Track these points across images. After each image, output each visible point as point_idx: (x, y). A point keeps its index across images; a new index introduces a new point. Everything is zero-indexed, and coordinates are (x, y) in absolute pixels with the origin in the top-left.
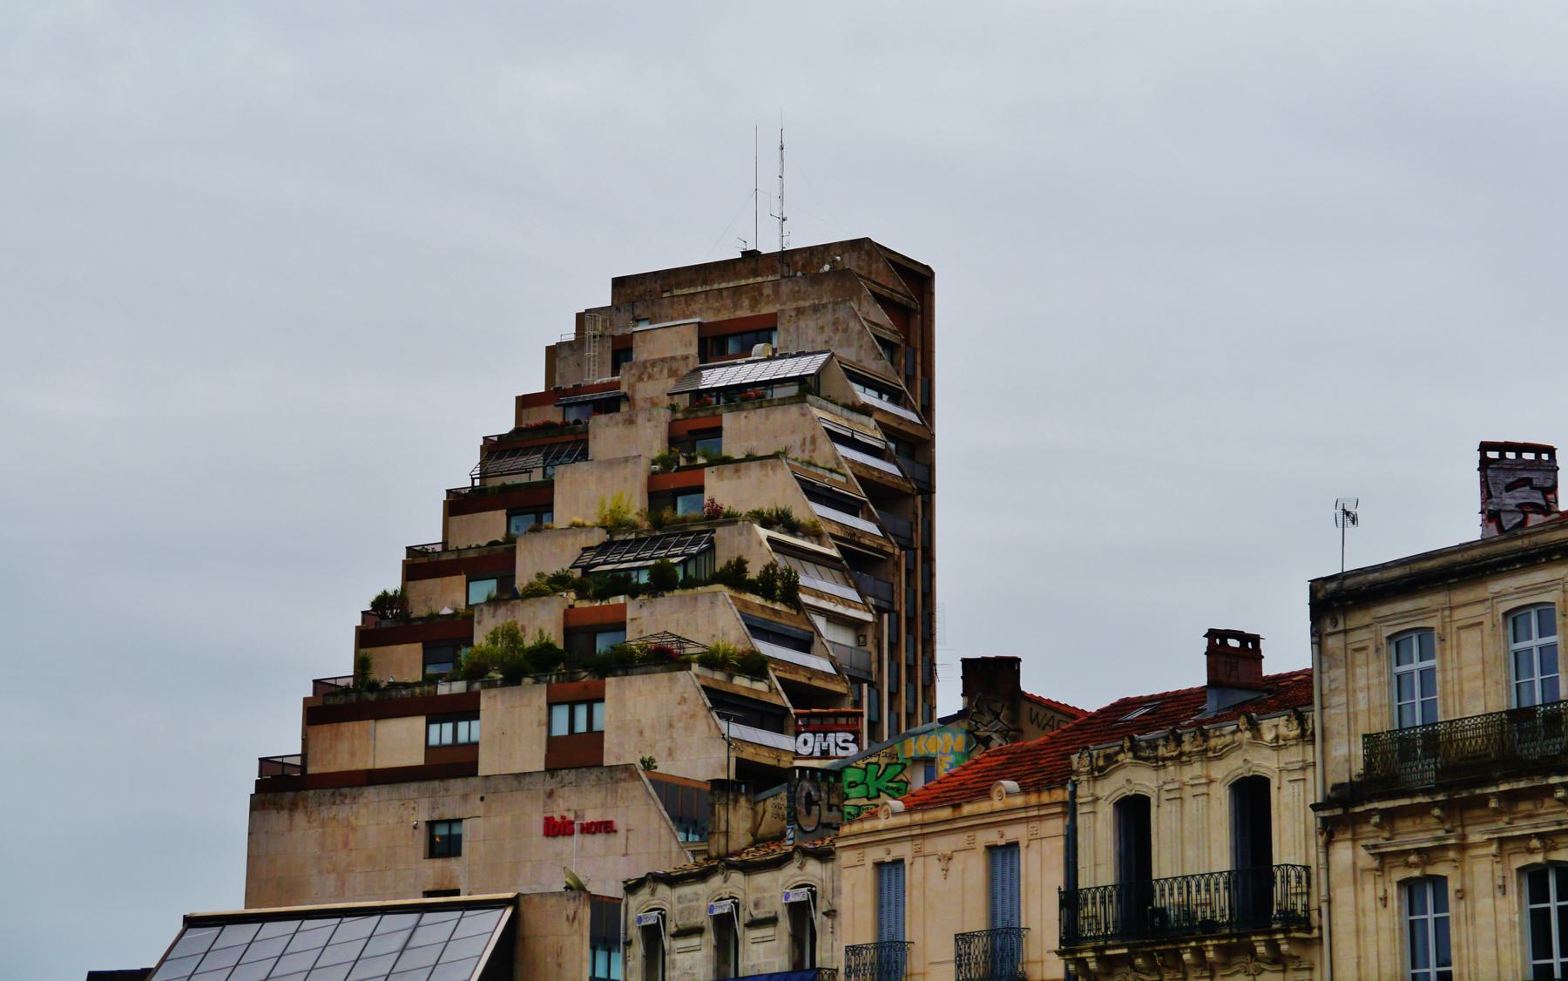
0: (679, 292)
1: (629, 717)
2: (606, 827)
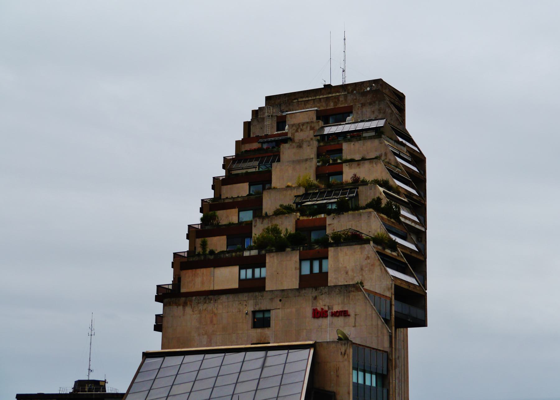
0: (301, 100)
1: (340, 265)
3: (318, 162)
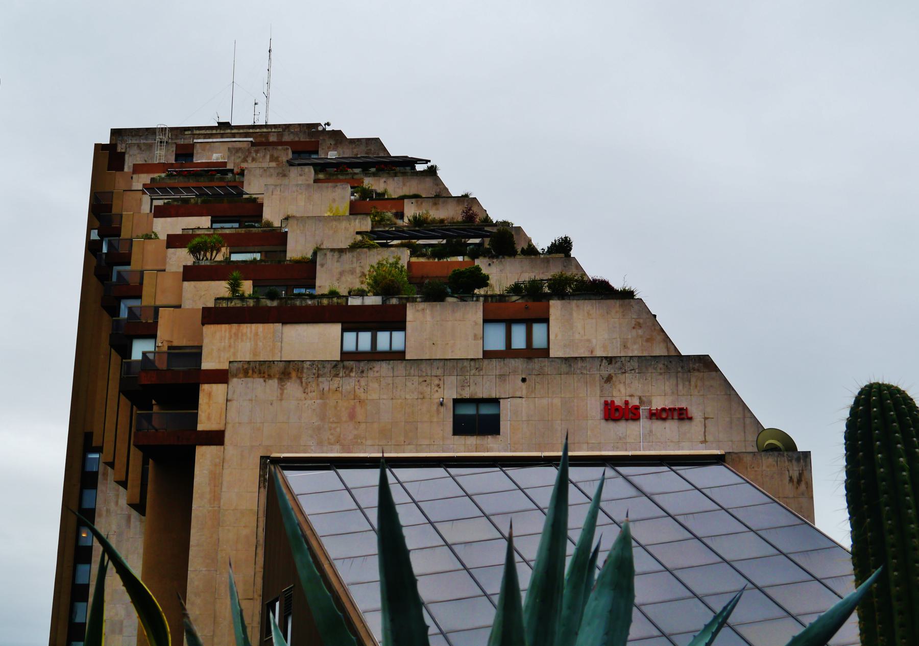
1: (577, 336)
3: (352, 194)
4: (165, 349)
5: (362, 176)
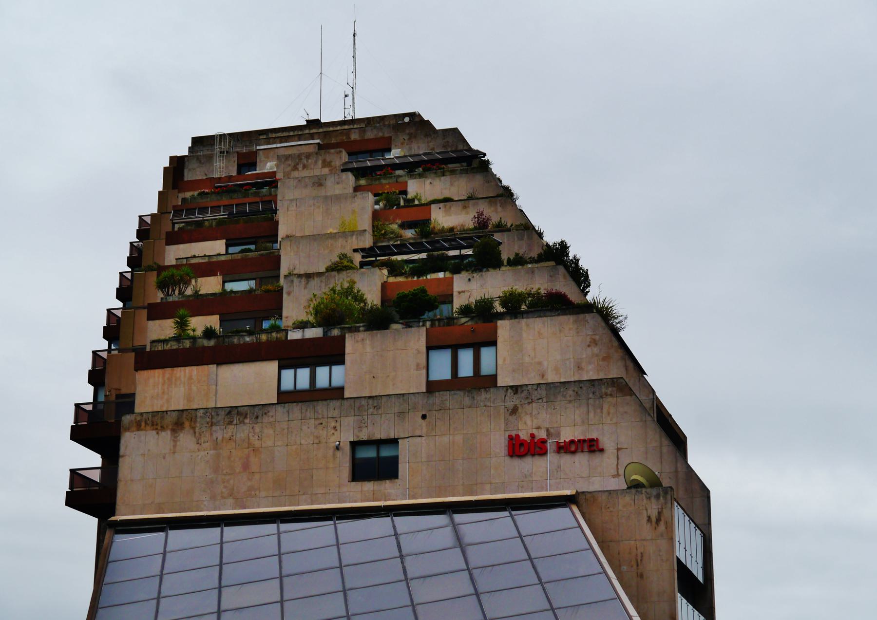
1: (527, 359)
2: (592, 446)
3: (377, 203)
4: (113, 398)
5: (406, 179)
